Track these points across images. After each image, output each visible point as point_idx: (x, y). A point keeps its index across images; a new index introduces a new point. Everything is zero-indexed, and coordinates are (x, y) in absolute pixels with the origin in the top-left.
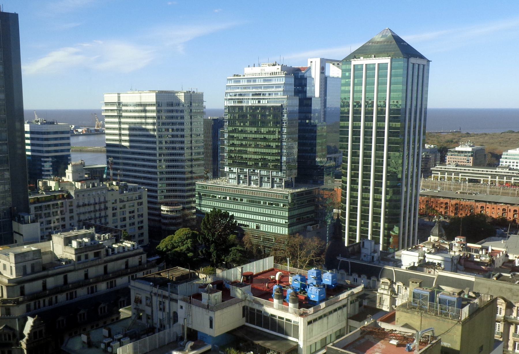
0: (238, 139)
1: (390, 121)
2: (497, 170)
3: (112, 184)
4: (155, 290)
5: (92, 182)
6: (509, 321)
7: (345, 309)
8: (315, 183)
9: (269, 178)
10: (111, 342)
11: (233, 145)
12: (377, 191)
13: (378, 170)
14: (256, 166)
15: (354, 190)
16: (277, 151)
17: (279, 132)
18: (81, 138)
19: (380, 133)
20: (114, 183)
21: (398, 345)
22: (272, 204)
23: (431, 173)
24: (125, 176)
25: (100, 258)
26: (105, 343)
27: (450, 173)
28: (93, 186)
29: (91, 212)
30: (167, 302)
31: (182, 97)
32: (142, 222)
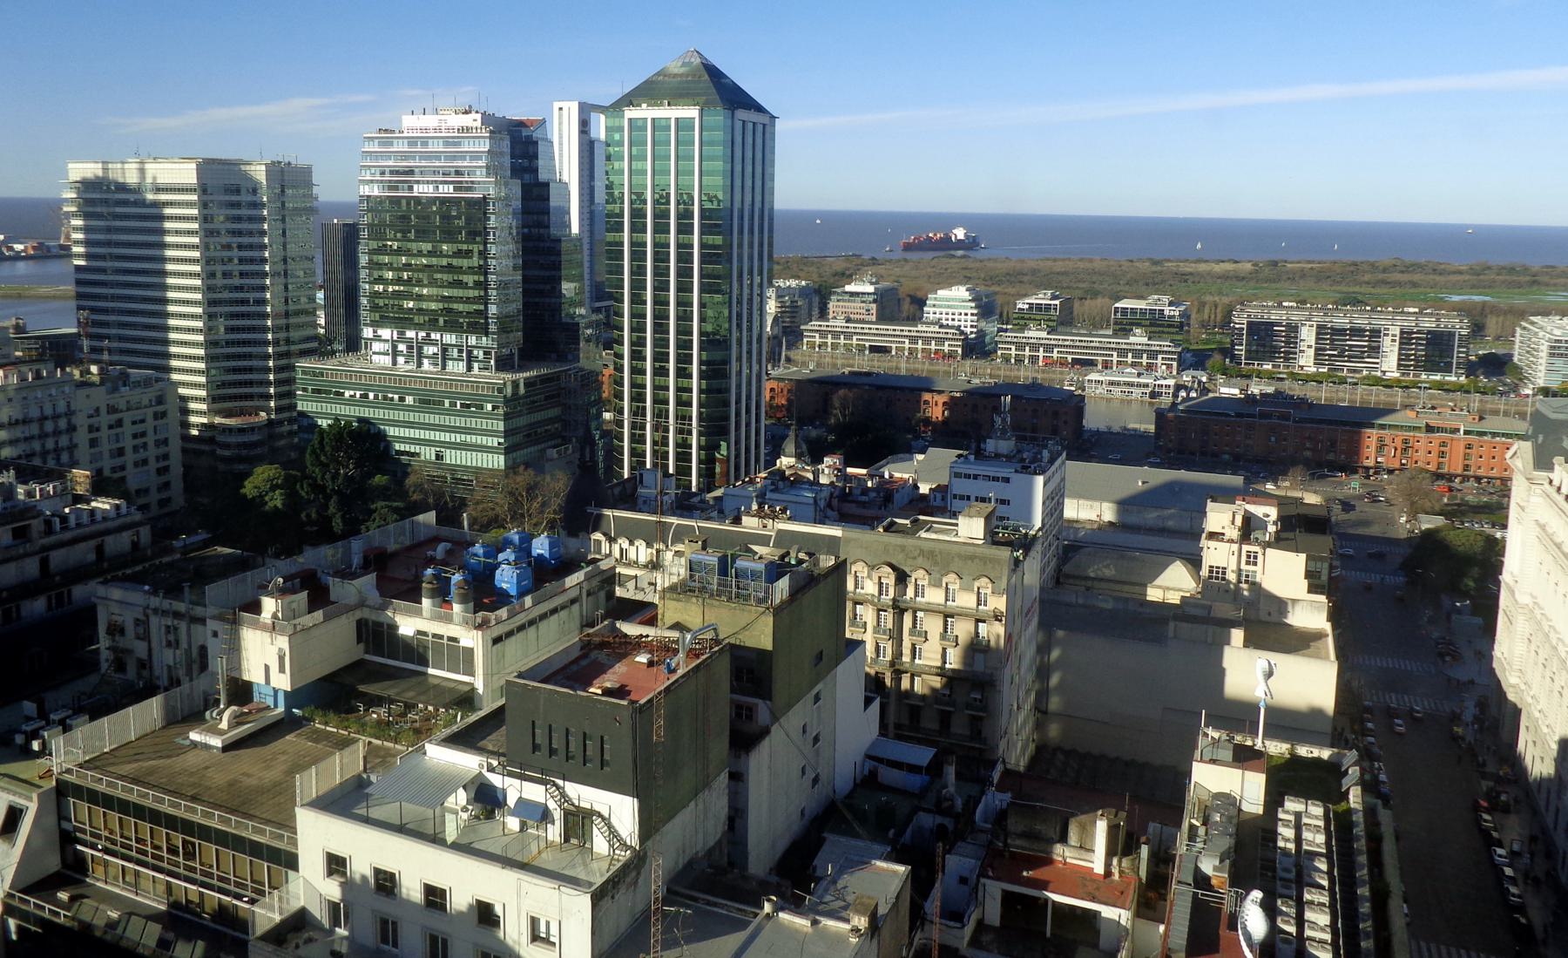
0: (390, 267)
1: (702, 233)
2: (920, 328)
3: (89, 372)
4: (155, 602)
5: (35, 367)
6: (902, 606)
7: (576, 607)
8: (562, 358)
9: (460, 351)
10: (42, 728)
11: (380, 280)
12: (683, 373)
13: (684, 332)
14: (432, 325)
15: (637, 371)
16: (476, 293)
17: (480, 253)
18: (21, 265)
19: (684, 257)
20: (94, 369)
21: (651, 664)
22: (468, 406)
23: (802, 336)
24: (122, 352)
25: (30, 541)
26: (25, 733)
27: (836, 335)
28: (38, 376)
29: (32, 437)
30: (183, 626)
31: (259, 173)
32: (166, 457)
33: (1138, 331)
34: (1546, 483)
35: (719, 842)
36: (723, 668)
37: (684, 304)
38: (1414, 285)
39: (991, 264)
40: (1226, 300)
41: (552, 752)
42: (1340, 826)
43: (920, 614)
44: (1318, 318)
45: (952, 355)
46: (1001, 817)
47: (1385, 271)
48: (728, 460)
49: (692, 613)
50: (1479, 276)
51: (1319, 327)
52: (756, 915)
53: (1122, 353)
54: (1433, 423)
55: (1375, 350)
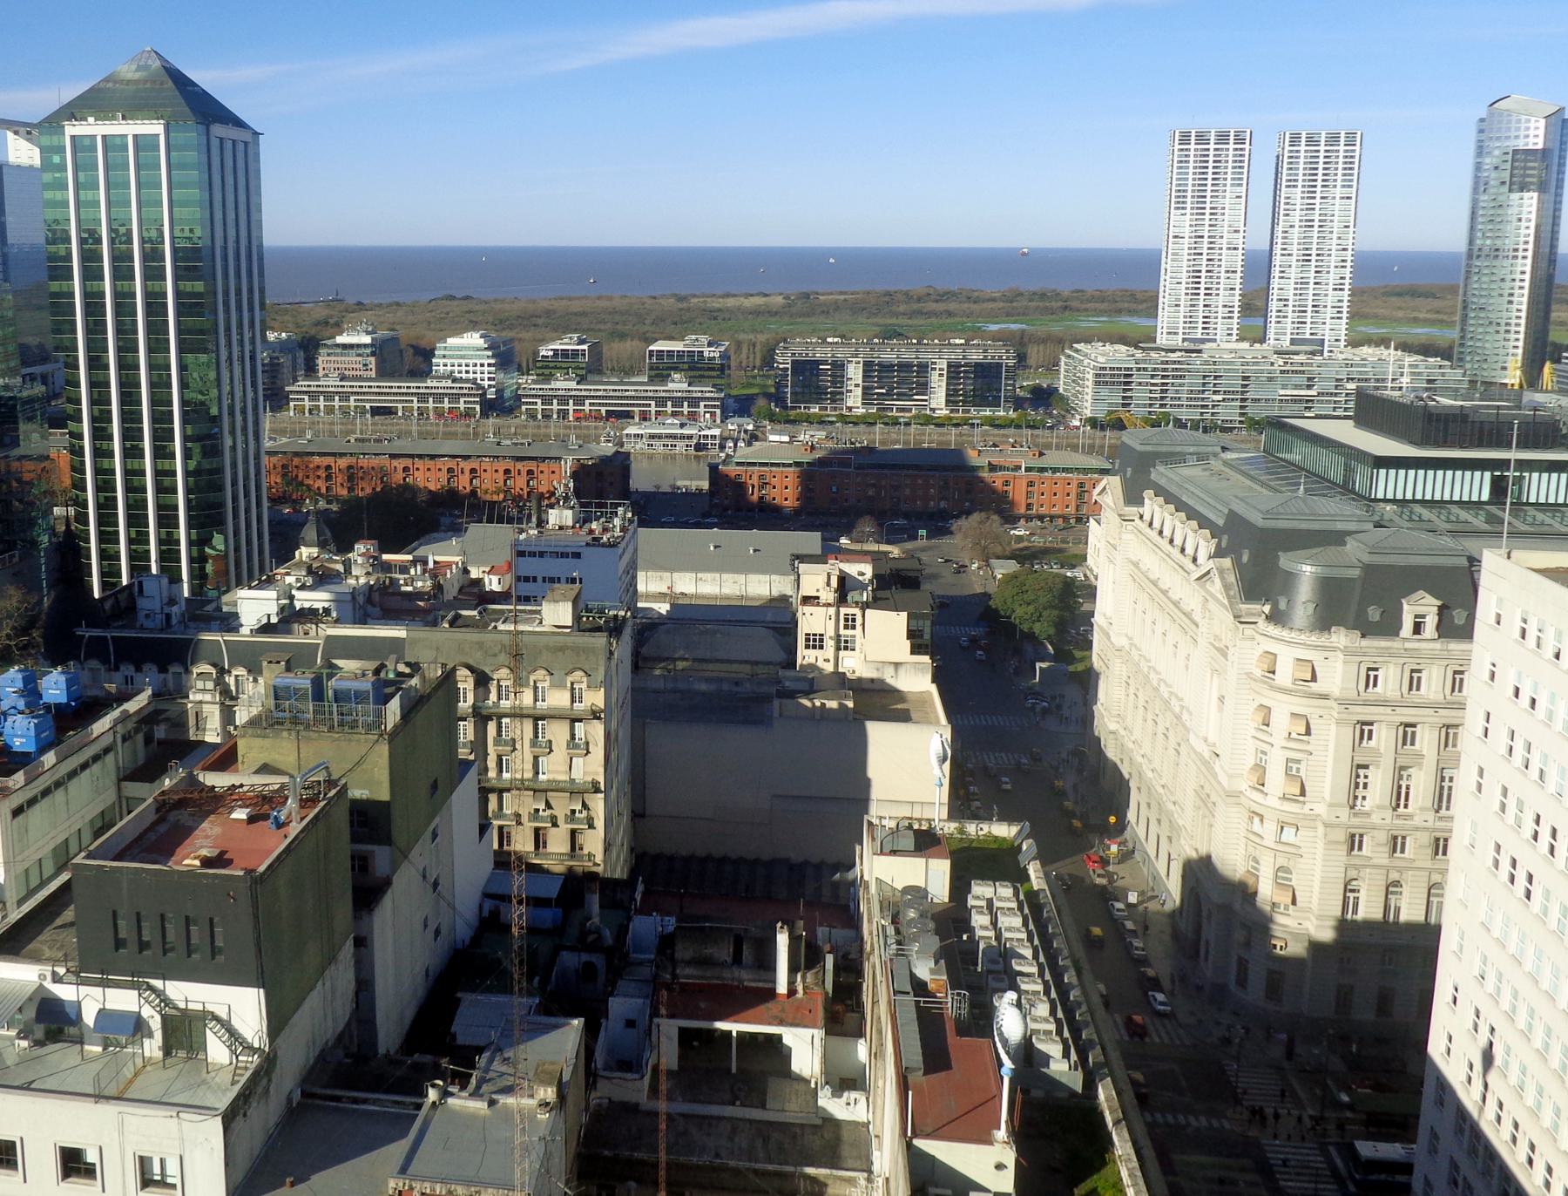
1: (176, 278)
2: (429, 383)
6: (484, 712)
15: (102, 453)
19: (155, 306)
21: (252, 820)
23: (288, 400)
27: (329, 396)
33: (677, 376)
34: (1137, 519)
35: (348, 1024)
36: (342, 818)
37: (158, 369)
38: (950, 314)
39: (498, 306)
40: (762, 338)
41: (143, 946)
42: (1032, 905)
43: (504, 721)
44: (864, 352)
45: (468, 414)
46: (666, 943)
47: (919, 300)
48: (226, 556)
49: (283, 749)
50: (1012, 304)
51: (866, 364)
52: (419, 1107)
53: (661, 402)
54: (995, 461)
55: (924, 387)
